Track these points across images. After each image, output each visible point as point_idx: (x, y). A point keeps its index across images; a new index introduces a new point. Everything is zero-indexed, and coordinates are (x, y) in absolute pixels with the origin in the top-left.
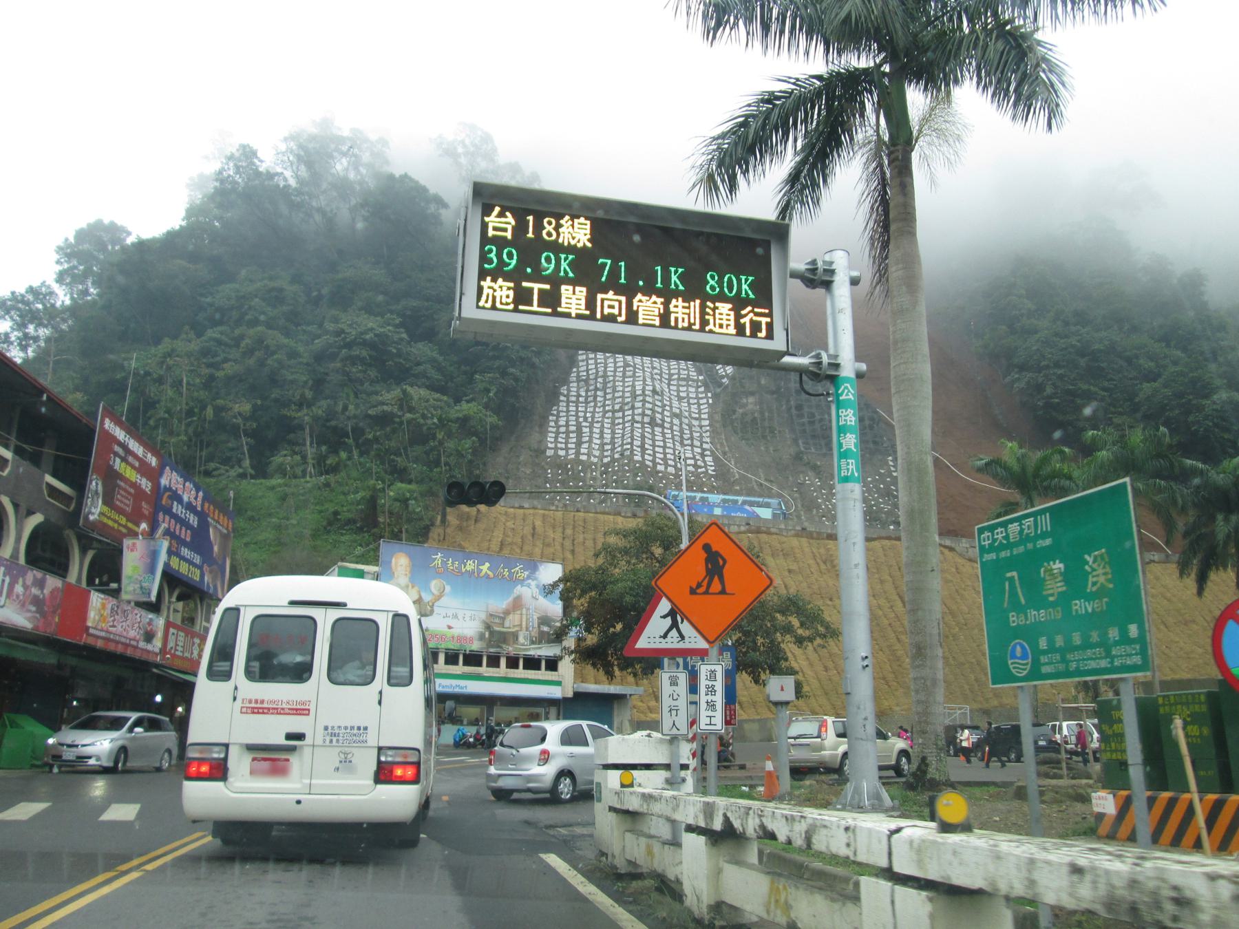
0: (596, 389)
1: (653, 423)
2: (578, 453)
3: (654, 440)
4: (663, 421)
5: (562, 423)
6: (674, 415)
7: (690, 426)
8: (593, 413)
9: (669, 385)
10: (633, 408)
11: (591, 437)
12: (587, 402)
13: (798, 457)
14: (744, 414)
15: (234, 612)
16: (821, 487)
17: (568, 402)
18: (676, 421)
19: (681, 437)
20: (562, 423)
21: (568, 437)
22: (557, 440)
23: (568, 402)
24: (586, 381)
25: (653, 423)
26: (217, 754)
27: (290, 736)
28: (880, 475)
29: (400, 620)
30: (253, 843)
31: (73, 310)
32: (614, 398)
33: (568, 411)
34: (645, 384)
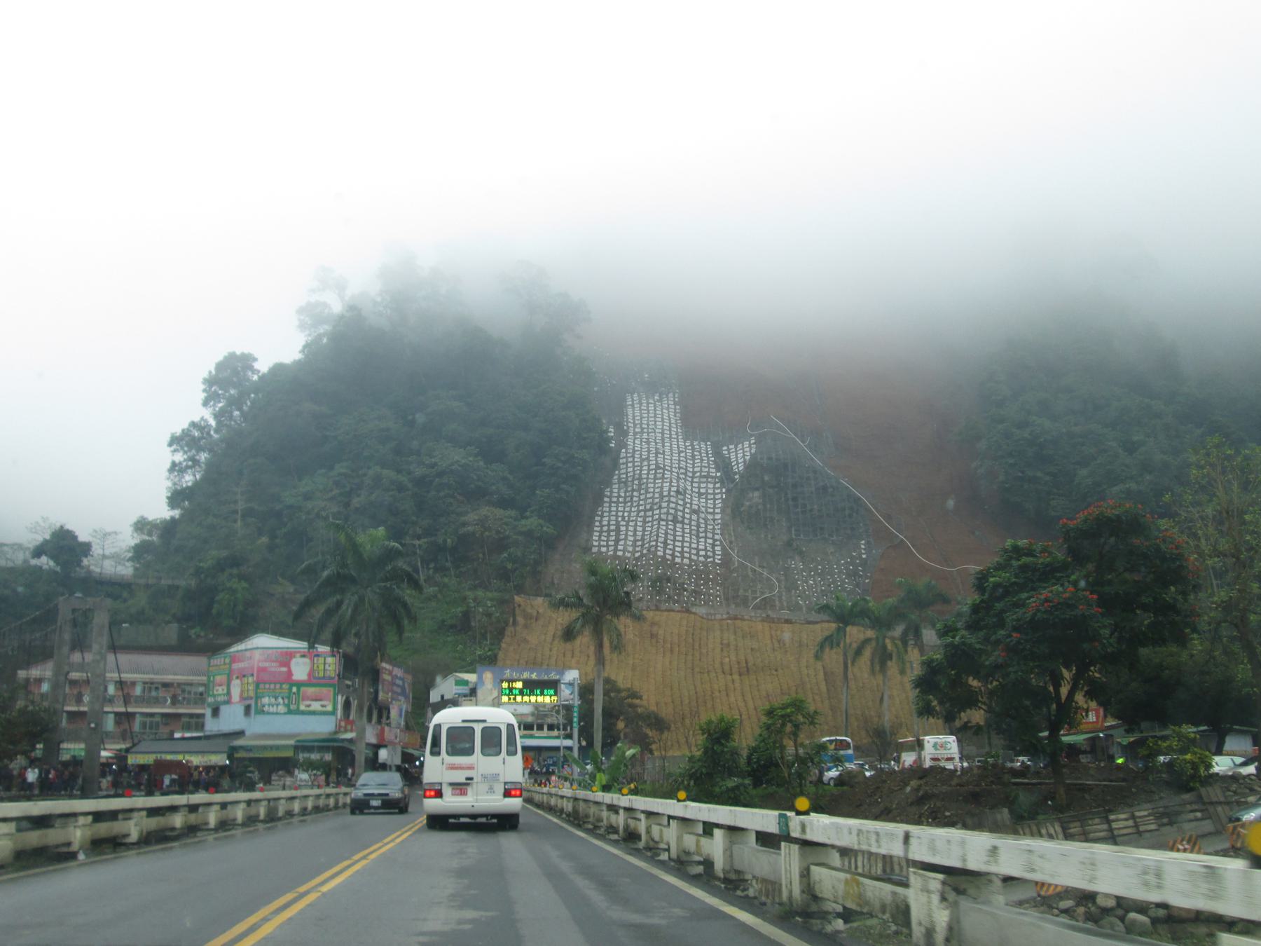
0: (633, 490)
1: (675, 521)
2: (616, 550)
3: (675, 536)
4: (683, 517)
5: (605, 523)
6: (696, 512)
7: (706, 519)
8: (630, 512)
9: (692, 482)
10: (660, 508)
11: (626, 535)
12: (625, 502)
13: (789, 544)
14: (750, 507)
15: (438, 727)
16: (803, 570)
17: (611, 502)
18: (694, 517)
19: (698, 531)
20: (605, 523)
21: (609, 535)
23: (611, 502)
24: (625, 483)
26: (437, 787)
28: (852, 557)
29: (510, 727)
30: (439, 822)
31: (221, 440)
32: (646, 499)
33: (610, 511)
34: (671, 486)
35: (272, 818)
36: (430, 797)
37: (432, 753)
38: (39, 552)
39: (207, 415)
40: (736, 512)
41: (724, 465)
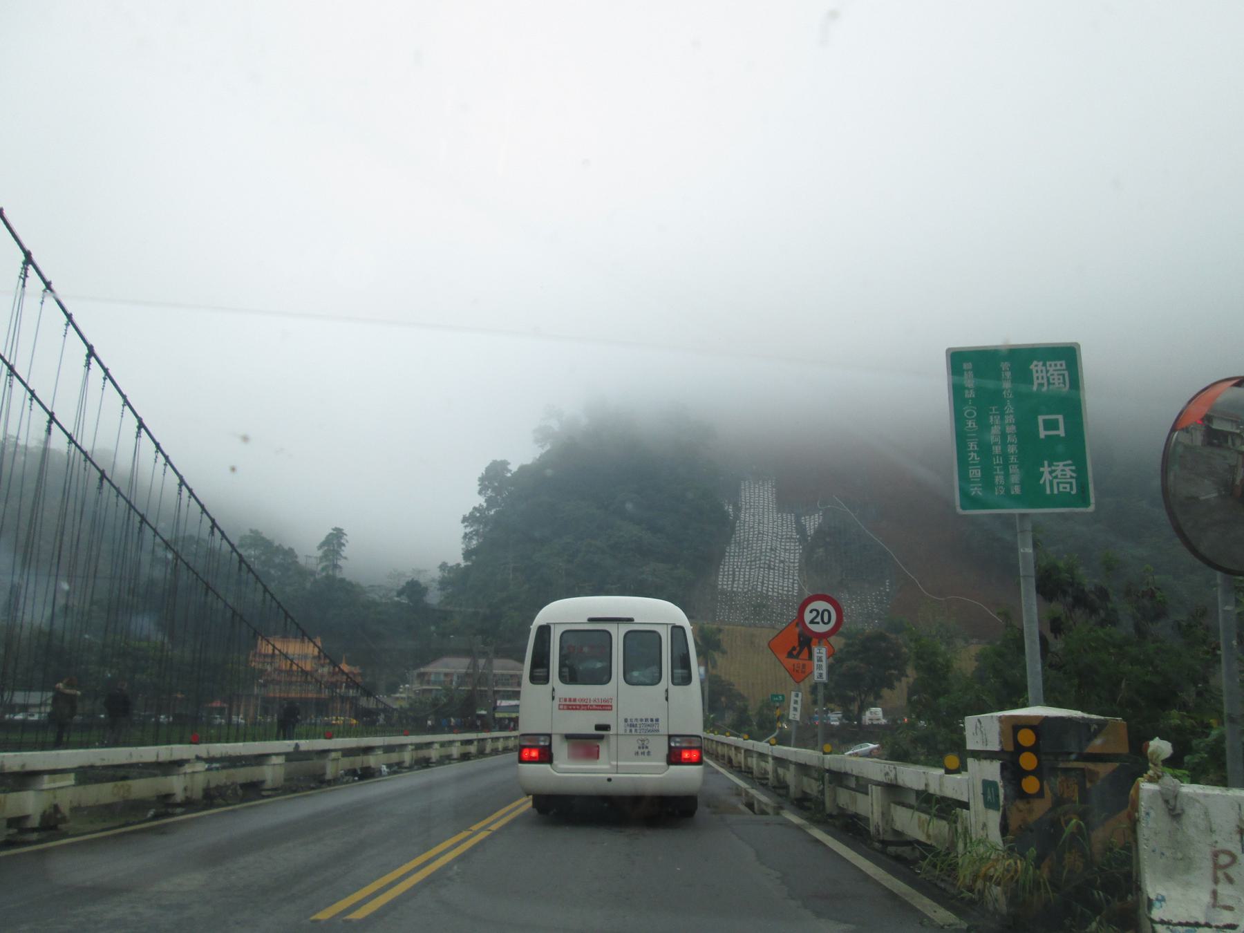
15: (544, 631)
22: (723, 582)
25: (769, 568)
27: (598, 727)
29: (677, 630)
35: (481, 753)
36: (531, 761)
37: (534, 679)
38: (400, 593)
39: (480, 501)
40: (809, 564)
41: (801, 530)
